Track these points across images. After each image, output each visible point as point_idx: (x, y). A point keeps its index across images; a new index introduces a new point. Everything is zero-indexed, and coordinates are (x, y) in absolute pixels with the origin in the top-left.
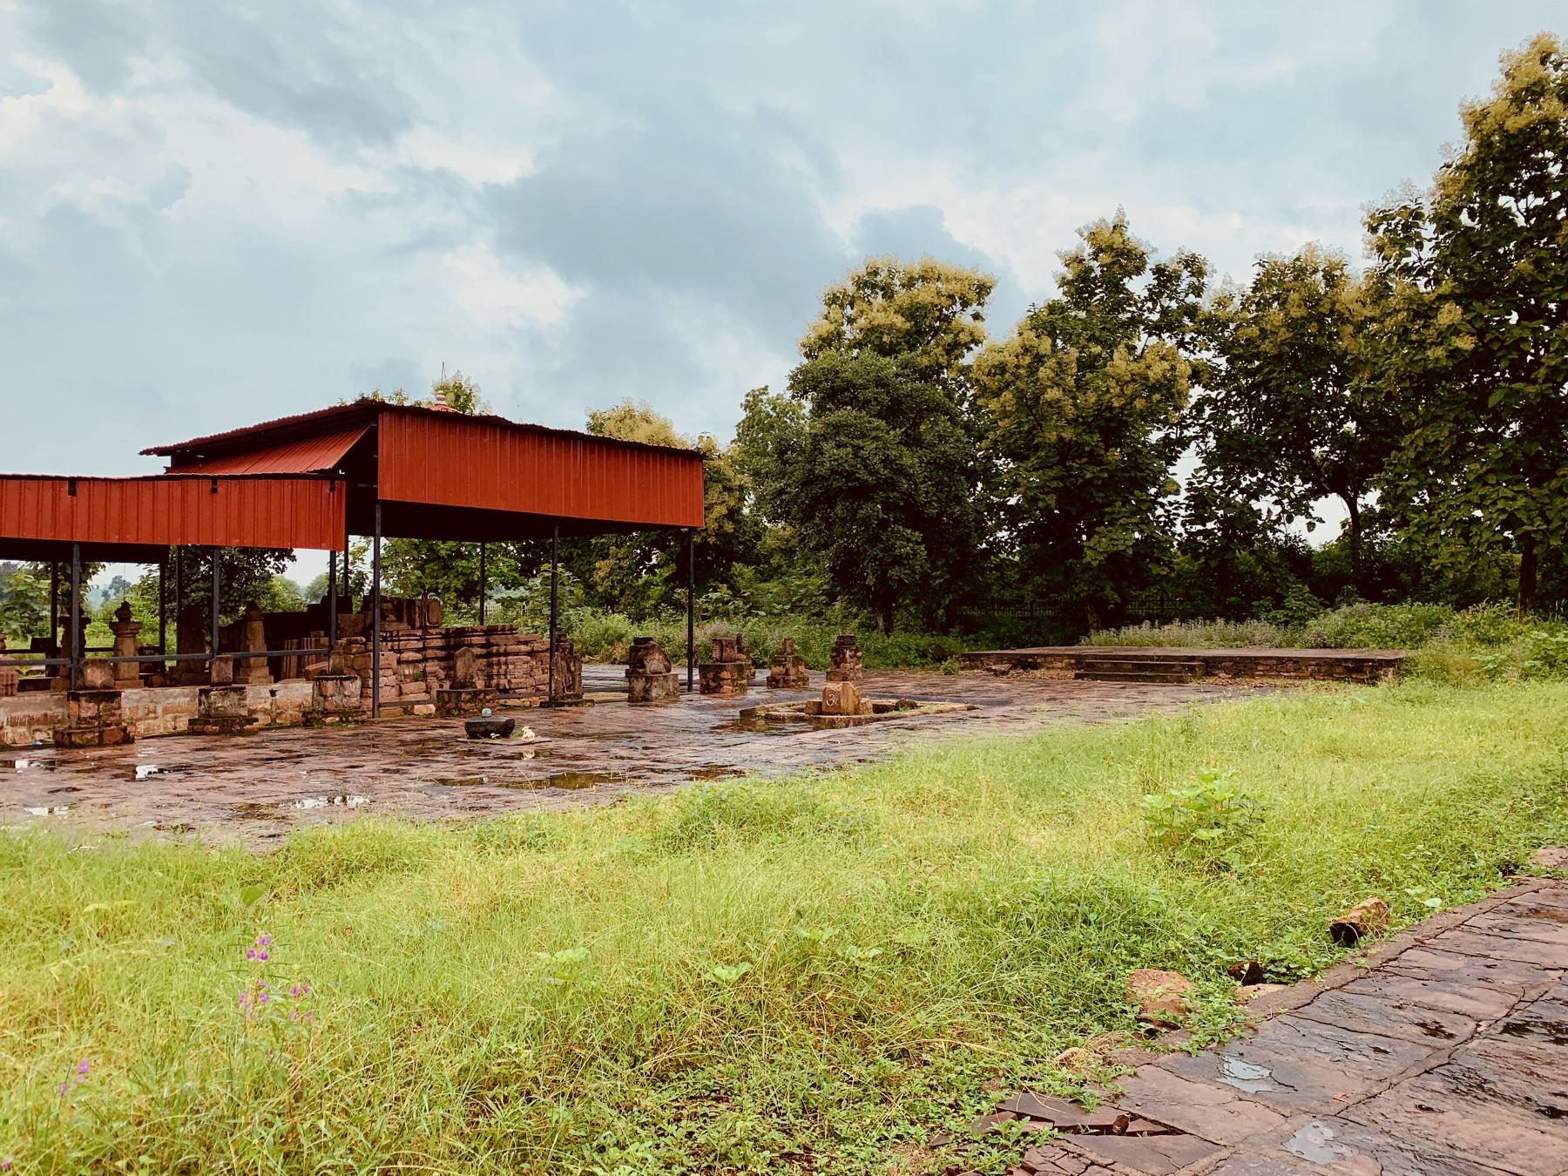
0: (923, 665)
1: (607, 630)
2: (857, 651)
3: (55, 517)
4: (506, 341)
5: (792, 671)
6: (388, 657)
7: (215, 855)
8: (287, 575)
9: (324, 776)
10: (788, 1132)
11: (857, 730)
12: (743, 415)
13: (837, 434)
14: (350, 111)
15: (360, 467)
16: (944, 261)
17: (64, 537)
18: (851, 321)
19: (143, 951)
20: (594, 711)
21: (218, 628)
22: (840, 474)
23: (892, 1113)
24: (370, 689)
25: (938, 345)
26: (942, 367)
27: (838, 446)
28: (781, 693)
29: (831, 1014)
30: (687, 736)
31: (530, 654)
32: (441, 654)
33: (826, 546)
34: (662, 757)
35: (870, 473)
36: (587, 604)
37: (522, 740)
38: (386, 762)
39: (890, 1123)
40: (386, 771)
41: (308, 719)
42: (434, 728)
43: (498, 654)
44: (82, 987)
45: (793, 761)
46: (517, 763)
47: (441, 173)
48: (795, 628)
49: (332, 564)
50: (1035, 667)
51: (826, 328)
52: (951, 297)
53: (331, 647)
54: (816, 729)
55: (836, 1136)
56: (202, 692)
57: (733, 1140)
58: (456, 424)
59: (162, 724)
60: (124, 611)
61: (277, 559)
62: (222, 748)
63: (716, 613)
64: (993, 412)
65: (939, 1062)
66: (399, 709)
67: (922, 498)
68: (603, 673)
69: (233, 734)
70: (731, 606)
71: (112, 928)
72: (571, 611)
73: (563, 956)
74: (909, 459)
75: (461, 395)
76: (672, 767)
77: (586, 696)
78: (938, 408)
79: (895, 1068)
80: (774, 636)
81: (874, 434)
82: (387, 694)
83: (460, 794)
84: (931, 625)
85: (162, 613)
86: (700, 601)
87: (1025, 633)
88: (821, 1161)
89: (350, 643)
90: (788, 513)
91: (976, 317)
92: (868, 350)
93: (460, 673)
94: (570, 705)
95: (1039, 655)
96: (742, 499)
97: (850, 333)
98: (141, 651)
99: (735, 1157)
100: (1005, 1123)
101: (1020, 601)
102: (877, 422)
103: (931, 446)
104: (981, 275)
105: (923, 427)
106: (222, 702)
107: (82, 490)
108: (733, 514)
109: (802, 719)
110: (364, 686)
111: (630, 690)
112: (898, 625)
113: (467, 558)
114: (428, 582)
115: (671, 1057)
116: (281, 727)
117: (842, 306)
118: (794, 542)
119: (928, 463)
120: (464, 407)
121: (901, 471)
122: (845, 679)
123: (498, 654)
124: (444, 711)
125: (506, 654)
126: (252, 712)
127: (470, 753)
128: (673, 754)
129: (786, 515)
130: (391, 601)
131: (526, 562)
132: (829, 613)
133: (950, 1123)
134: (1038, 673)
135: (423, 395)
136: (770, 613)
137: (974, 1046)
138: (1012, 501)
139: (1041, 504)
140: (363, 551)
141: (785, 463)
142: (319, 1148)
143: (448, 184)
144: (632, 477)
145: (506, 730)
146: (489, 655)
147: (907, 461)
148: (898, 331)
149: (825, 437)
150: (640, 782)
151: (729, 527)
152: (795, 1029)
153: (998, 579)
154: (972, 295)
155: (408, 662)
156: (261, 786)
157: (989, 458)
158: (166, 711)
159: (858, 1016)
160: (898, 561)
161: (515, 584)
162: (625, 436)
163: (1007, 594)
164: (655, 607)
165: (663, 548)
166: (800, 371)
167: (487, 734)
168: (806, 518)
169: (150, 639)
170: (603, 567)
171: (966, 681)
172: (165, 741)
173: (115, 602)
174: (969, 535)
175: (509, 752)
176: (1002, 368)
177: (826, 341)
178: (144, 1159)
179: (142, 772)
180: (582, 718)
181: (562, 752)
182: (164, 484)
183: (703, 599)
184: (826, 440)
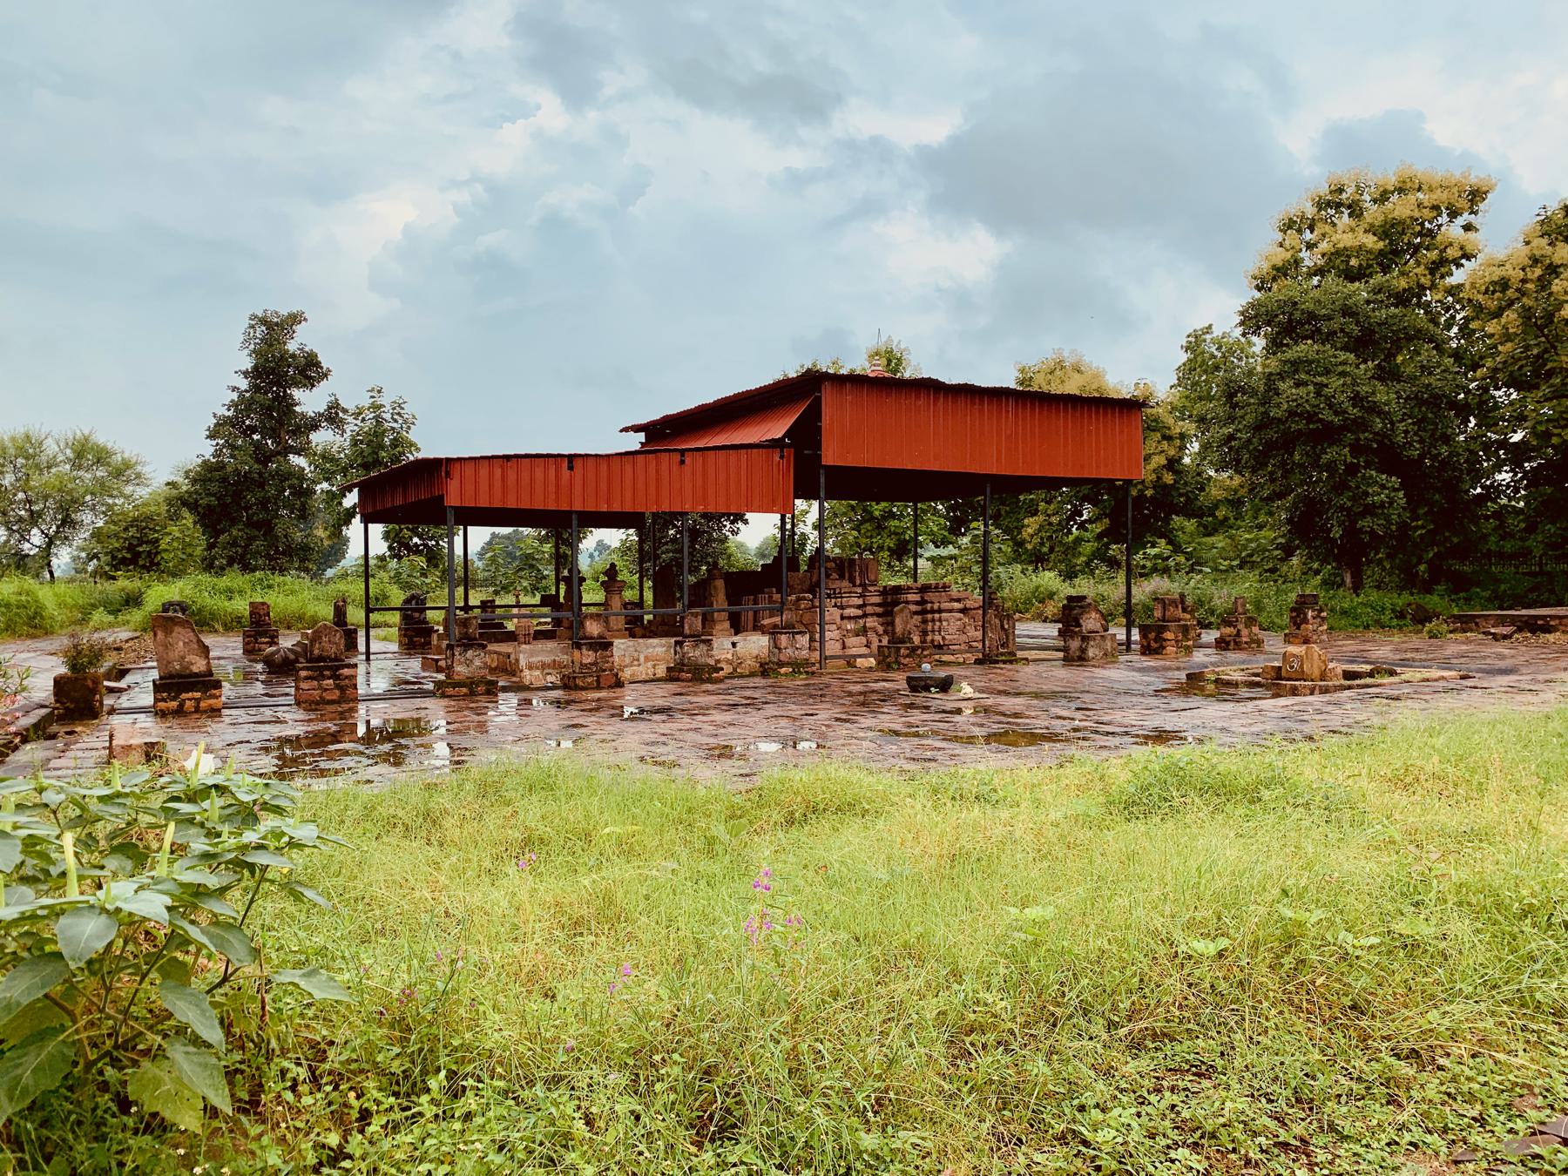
0: (1401, 628)
1: (1037, 588)
2: (1321, 610)
3: (557, 486)
4: (936, 303)
5: (1245, 632)
6: (832, 614)
7: (701, 791)
8: (739, 538)
9: (783, 722)
10: (1281, 1121)
11: (1327, 697)
12: (1184, 357)
13: (1296, 371)
14: (792, 97)
15: (805, 437)
16: (1422, 168)
17: (565, 507)
18: (1310, 246)
19: (654, 872)
20: (1029, 669)
21: (687, 585)
22: (1300, 415)
23: (1403, 1117)
24: (818, 642)
25: (1418, 263)
26: (1425, 289)
27: (1298, 385)
28: (1232, 656)
29: (1322, 1001)
30: (1128, 698)
31: (962, 611)
32: (879, 610)
33: (1281, 496)
34: (1106, 718)
35: (1336, 413)
36: (1015, 560)
37: (961, 695)
38: (836, 711)
39: (1402, 1128)
40: (837, 719)
41: (765, 669)
42: (877, 681)
43: (933, 611)
44: (609, 900)
45: (1254, 729)
46: (957, 718)
47: (876, 141)
48: (1246, 586)
49: (782, 528)
50: (1548, 629)
51: (1281, 256)
52: (1436, 208)
53: (782, 603)
54: (1276, 696)
55: (1337, 1132)
56: (677, 643)
57: (1222, 1120)
58: (888, 387)
59: (644, 671)
60: (612, 571)
61: (732, 522)
62: (696, 693)
63: (1155, 569)
64: (1491, 336)
65: (1457, 1069)
66: (842, 662)
67: (1400, 439)
68: (1036, 631)
69: (704, 681)
70: (1171, 563)
71: (627, 850)
72: (1001, 569)
73: (1033, 913)
74: (1383, 395)
75: (892, 359)
76: (1118, 730)
77: (1020, 654)
78: (1419, 335)
79: (1406, 1069)
80: (1222, 596)
81: (1340, 368)
82: (832, 648)
83: (907, 745)
84: (1410, 581)
85: (641, 572)
86: (1138, 557)
87: (1531, 590)
88: (1321, 1157)
89: (799, 599)
90: (1238, 461)
91: (1468, 228)
92: (1330, 278)
93: (899, 629)
94: (1004, 662)
95: (1553, 617)
96: (1182, 448)
97: (1309, 259)
98: (625, 605)
99: (1224, 1138)
100: (1550, 1147)
101: (1525, 554)
102: (1343, 356)
103: (1412, 379)
104: (1474, 178)
105: (1400, 359)
106: (694, 653)
107: (578, 464)
108: (1173, 464)
109: (1258, 685)
110: (812, 640)
111: (1065, 649)
112: (1368, 582)
113: (900, 517)
114: (864, 542)
115: (1164, 1023)
116: (742, 676)
117: (1300, 231)
118: (1242, 492)
119: (1408, 398)
120: (895, 371)
121: (1375, 409)
122: (1306, 641)
123: (933, 611)
124: (886, 662)
125: (940, 611)
126: (718, 661)
127: (911, 706)
128: (1117, 716)
129: (1236, 465)
130: (834, 560)
131: (954, 520)
132: (1285, 568)
133: (1475, 1138)
134: (1551, 637)
135: (857, 362)
136: (1215, 569)
137: (1501, 1056)
138: (1516, 437)
139: (1555, 440)
140: (809, 512)
141: (1234, 406)
142: (818, 1068)
143: (881, 150)
144: (1066, 427)
145: (945, 685)
146: (924, 612)
147: (1381, 397)
148: (1369, 252)
149: (1281, 376)
150: (1086, 744)
151: (1169, 478)
152: (1281, 1013)
153: (1495, 529)
154: (1462, 203)
155: (850, 618)
156: (731, 729)
157: (1486, 390)
158: (647, 659)
159: (1353, 1008)
160: (1370, 510)
161: (944, 543)
162: (1056, 389)
163: (1508, 546)
164: (1088, 564)
165: (1095, 502)
166: (1252, 305)
167: (927, 689)
168: (1259, 463)
169: (630, 595)
170: (1031, 524)
171: (1455, 646)
172: (648, 686)
173: (602, 563)
174: (1460, 480)
175: (949, 706)
176: (1504, 284)
177: (1281, 271)
178: (676, 1056)
179: (628, 711)
180: (1017, 676)
181: (1001, 709)
182: (641, 458)
183: (1140, 555)
184: (1283, 379)
